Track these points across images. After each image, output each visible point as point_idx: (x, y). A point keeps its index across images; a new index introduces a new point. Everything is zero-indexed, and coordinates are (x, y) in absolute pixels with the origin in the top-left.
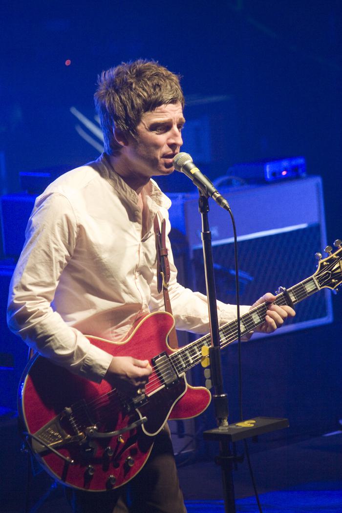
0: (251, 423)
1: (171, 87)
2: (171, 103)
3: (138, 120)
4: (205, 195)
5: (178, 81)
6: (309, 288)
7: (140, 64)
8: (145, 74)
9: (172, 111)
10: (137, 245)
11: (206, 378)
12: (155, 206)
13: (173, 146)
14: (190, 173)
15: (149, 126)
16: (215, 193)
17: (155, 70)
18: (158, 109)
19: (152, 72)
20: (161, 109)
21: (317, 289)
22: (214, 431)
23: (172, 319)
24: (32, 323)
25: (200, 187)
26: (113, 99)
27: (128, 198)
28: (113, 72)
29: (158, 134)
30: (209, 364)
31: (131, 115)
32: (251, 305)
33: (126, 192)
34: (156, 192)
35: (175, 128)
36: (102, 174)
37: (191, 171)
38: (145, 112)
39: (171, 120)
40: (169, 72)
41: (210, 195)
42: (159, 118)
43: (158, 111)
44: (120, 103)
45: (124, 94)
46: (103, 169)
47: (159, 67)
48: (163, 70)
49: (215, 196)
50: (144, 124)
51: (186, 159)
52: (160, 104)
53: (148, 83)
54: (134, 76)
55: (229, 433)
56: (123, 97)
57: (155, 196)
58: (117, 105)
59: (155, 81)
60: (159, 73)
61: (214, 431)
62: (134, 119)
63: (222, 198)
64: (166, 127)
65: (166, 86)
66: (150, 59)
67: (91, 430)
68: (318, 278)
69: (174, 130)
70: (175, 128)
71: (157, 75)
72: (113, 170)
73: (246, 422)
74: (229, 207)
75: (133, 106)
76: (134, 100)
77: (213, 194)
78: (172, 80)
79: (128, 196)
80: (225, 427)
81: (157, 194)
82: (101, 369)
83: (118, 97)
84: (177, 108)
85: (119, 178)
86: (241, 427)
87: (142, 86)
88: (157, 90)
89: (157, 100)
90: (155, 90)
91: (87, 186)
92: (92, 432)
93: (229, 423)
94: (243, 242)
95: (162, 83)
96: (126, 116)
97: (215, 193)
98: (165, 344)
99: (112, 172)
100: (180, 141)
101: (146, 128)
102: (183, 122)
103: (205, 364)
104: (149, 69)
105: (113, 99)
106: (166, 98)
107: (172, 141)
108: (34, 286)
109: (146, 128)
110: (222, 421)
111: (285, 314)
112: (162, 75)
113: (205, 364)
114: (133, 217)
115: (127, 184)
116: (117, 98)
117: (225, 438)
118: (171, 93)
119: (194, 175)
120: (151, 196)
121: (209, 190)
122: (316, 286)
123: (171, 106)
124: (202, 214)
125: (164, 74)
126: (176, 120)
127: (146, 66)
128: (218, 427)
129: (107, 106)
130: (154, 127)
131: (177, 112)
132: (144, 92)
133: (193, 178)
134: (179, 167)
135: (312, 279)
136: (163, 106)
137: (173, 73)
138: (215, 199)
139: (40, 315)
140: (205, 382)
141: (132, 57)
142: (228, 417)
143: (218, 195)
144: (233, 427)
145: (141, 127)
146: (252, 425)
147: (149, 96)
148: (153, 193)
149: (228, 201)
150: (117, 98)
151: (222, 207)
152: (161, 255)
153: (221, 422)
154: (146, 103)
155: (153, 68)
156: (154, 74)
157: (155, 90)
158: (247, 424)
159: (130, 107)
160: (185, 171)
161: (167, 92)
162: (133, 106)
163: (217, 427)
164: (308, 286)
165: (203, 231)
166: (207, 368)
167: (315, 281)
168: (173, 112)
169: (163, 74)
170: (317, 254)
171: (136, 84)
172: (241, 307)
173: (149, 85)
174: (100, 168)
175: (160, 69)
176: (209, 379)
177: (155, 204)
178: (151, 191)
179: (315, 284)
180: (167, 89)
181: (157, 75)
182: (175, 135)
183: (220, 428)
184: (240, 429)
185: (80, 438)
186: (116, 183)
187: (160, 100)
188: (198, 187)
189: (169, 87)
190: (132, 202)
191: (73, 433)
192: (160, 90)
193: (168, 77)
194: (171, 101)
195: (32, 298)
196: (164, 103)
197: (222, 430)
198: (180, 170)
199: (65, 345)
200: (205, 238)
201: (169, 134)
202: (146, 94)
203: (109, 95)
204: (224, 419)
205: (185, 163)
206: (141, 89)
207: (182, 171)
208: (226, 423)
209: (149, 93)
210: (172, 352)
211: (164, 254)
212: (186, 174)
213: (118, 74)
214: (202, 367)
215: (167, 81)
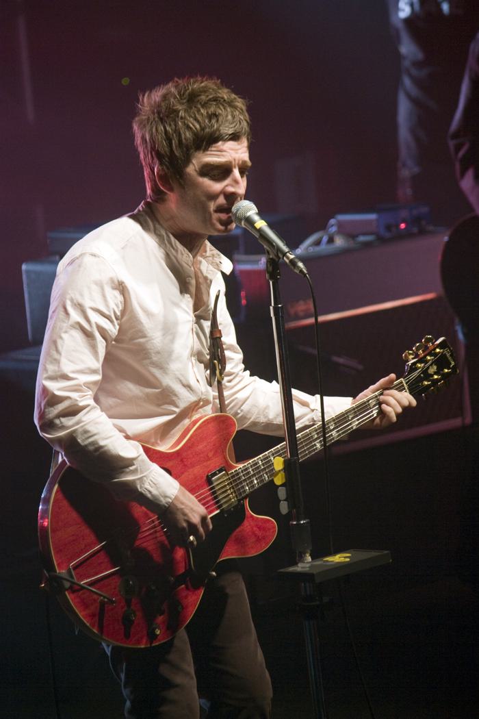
0: (345, 557)
1: (234, 117)
3: (188, 161)
4: (274, 257)
5: (244, 108)
7: (196, 85)
8: (199, 98)
9: (232, 149)
11: (280, 498)
12: (211, 271)
14: (255, 228)
17: (213, 93)
19: (208, 96)
20: (217, 147)
22: (291, 569)
23: (230, 418)
24: (63, 427)
26: (156, 129)
27: (180, 260)
28: (157, 95)
30: (284, 481)
31: (177, 153)
32: (354, 395)
33: (177, 251)
34: (211, 252)
35: (236, 172)
36: (145, 226)
37: (256, 225)
38: (196, 151)
39: (231, 162)
40: (233, 96)
41: (281, 256)
43: (213, 149)
44: (163, 135)
45: (170, 125)
46: (146, 222)
47: (220, 89)
48: (225, 94)
49: (288, 258)
50: (194, 164)
51: (248, 208)
53: (202, 111)
54: (185, 101)
55: (311, 572)
56: (168, 128)
57: (211, 258)
58: (160, 138)
59: (212, 110)
60: (219, 97)
61: (291, 569)
63: (296, 260)
64: (223, 172)
65: (227, 116)
66: (210, 77)
69: (234, 176)
70: (236, 172)
71: (215, 99)
72: (159, 224)
73: (338, 556)
74: (305, 272)
76: (182, 132)
77: (284, 254)
78: (235, 107)
79: (179, 256)
80: (306, 563)
85: (166, 234)
87: (193, 116)
88: (213, 121)
90: (210, 121)
91: (126, 245)
94: (287, 245)
95: (220, 112)
97: (288, 254)
99: (157, 226)
101: (196, 170)
102: (247, 166)
103: (278, 481)
104: (205, 92)
107: (231, 189)
108: (69, 366)
111: (406, 403)
112: (222, 100)
113: (278, 481)
114: (184, 288)
115: (179, 241)
117: (306, 577)
118: (231, 126)
119: (260, 231)
121: (279, 249)
124: (271, 283)
125: (226, 97)
127: (202, 87)
131: (240, 151)
132: (192, 123)
133: (259, 234)
136: (220, 143)
137: (240, 98)
138: (287, 261)
139: (73, 411)
142: (311, 551)
144: (318, 562)
145: (191, 169)
146: (348, 560)
147: (203, 129)
148: (208, 253)
149: (304, 264)
151: (298, 272)
152: (215, 336)
155: (211, 90)
157: (210, 121)
158: (339, 558)
159: (177, 142)
160: (248, 226)
163: (295, 564)
165: (273, 305)
166: (281, 485)
168: (236, 152)
169: (223, 98)
171: (186, 111)
172: (325, 398)
173: (202, 114)
174: (141, 219)
175: (220, 91)
177: (211, 267)
180: (227, 121)
181: (214, 101)
182: (236, 182)
183: (299, 565)
184: (332, 565)
186: (164, 240)
187: (216, 135)
188: (265, 247)
189: (230, 117)
190: (185, 265)
192: (217, 121)
193: (230, 104)
194: (230, 137)
195: (76, 389)
197: (302, 568)
199: (174, 433)
200: (275, 315)
202: (198, 126)
204: (305, 553)
205: (248, 214)
208: (309, 559)
209: (203, 125)
210: (236, 467)
211: (218, 336)
212: (250, 229)
213: (165, 97)
214: (275, 485)
215: (229, 110)
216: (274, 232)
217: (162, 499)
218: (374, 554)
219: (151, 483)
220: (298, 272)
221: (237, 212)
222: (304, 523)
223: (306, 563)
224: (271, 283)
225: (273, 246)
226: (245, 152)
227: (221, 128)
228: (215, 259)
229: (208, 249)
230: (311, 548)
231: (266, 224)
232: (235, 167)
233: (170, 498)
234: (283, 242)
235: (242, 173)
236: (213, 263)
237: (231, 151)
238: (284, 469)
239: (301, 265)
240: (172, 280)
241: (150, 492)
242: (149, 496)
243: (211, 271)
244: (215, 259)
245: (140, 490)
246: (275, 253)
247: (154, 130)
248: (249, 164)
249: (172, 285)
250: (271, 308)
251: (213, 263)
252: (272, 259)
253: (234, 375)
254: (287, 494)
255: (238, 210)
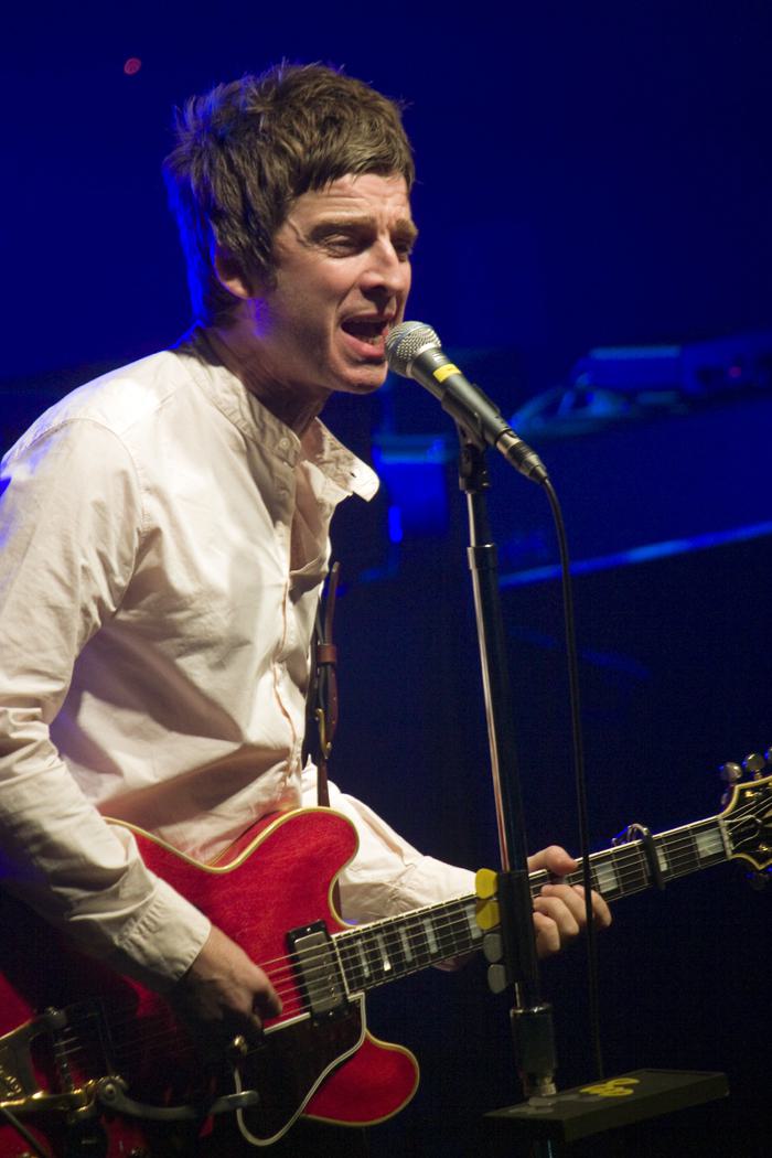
0: (626, 1087)
2: (370, 170)
3: (279, 218)
4: (476, 443)
6: (706, 845)
7: (283, 73)
10: (280, 586)
12: (332, 490)
13: (377, 293)
14: (435, 380)
15: (308, 234)
16: (506, 436)
18: (332, 187)
21: (723, 854)
22: (513, 1111)
25: (464, 419)
26: (211, 164)
29: (330, 256)
31: (260, 203)
34: (333, 453)
35: (385, 242)
39: (373, 220)
40: (372, 93)
41: (490, 439)
42: (334, 210)
43: (334, 191)
45: (239, 149)
48: (355, 87)
49: (506, 444)
50: (294, 229)
51: (422, 339)
52: (340, 171)
53: (306, 112)
57: (332, 466)
61: (513, 1111)
62: (265, 219)
64: (359, 237)
67: (109, 1086)
68: (731, 825)
73: (611, 1084)
74: (543, 473)
75: (262, 181)
76: (264, 161)
77: (498, 436)
78: (379, 111)
80: (546, 1098)
81: (337, 460)
82: (188, 941)
83: (222, 157)
84: (390, 190)
86: (597, 1099)
88: (331, 134)
89: (328, 159)
90: (323, 132)
92: (111, 1092)
93: (559, 1089)
96: (244, 206)
97: (506, 436)
98: (405, 1044)
100: (400, 276)
102: (408, 235)
105: (211, 164)
106: (355, 157)
107: (375, 278)
109: (300, 241)
110: (538, 1082)
116: (221, 163)
117: (546, 1129)
119: (445, 385)
120: (320, 463)
121: (486, 426)
122: (723, 846)
123: (370, 180)
124: (469, 497)
126: (386, 222)
128: (527, 1099)
129: (193, 186)
130: (322, 234)
131: (389, 200)
134: (403, 362)
135: (715, 824)
136: (347, 178)
138: (504, 450)
140: (487, 969)
141: (257, 63)
143: (515, 441)
144: (571, 1097)
145: (290, 236)
146: (630, 1092)
147: (309, 150)
148: (326, 456)
149: (542, 458)
150: (221, 163)
153: (535, 1085)
154: (299, 171)
156: (326, 90)
158: (612, 1089)
161: (359, 140)
162: (262, 181)
163: (522, 1099)
164: (707, 839)
165: (473, 543)
166: (491, 931)
167: (724, 830)
168: (381, 198)
170: (729, 765)
171: (272, 116)
176: (498, 963)
177: (332, 484)
178: (321, 451)
179: (722, 838)
183: (533, 1102)
185: (74, 1103)
187: (337, 162)
191: (53, 1086)
194: (370, 164)
196: (350, 169)
197: (538, 1108)
198: (405, 371)
200: (478, 565)
201: (365, 258)
203: (200, 156)
204: (544, 1076)
205: (422, 350)
206: (284, 132)
207: (409, 372)
208: (551, 1089)
210: (342, 929)
212: (423, 381)
216: (474, 388)
217: (165, 964)
218: (686, 1079)
219: (148, 922)
220: (527, 474)
221: (395, 347)
222: (539, 1012)
223: (546, 1098)
224: (469, 497)
225: (475, 419)
226: (403, 205)
227: (349, 146)
228: (341, 467)
229: (327, 447)
230: (555, 1065)
231: (458, 371)
232: (383, 233)
233: (185, 963)
234: (494, 409)
235: (399, 248)
236: (336, 475)
237: (372, 197)
238: (497, 894)
239: (533, 458)
240: (251, 495)
241: (140, 948)
242: (138, 956)
243: (332, 490)
244: (341, 467)
245: (117, 942)
246: (478, 433)
247: (205, 166)
248: (413, 230)
249: (257, 511)
250: (470, 550)
251: (336, 475)
252: (471, 446)
253: (366, 168)
254: (504, 949)
255: (398, 342)
